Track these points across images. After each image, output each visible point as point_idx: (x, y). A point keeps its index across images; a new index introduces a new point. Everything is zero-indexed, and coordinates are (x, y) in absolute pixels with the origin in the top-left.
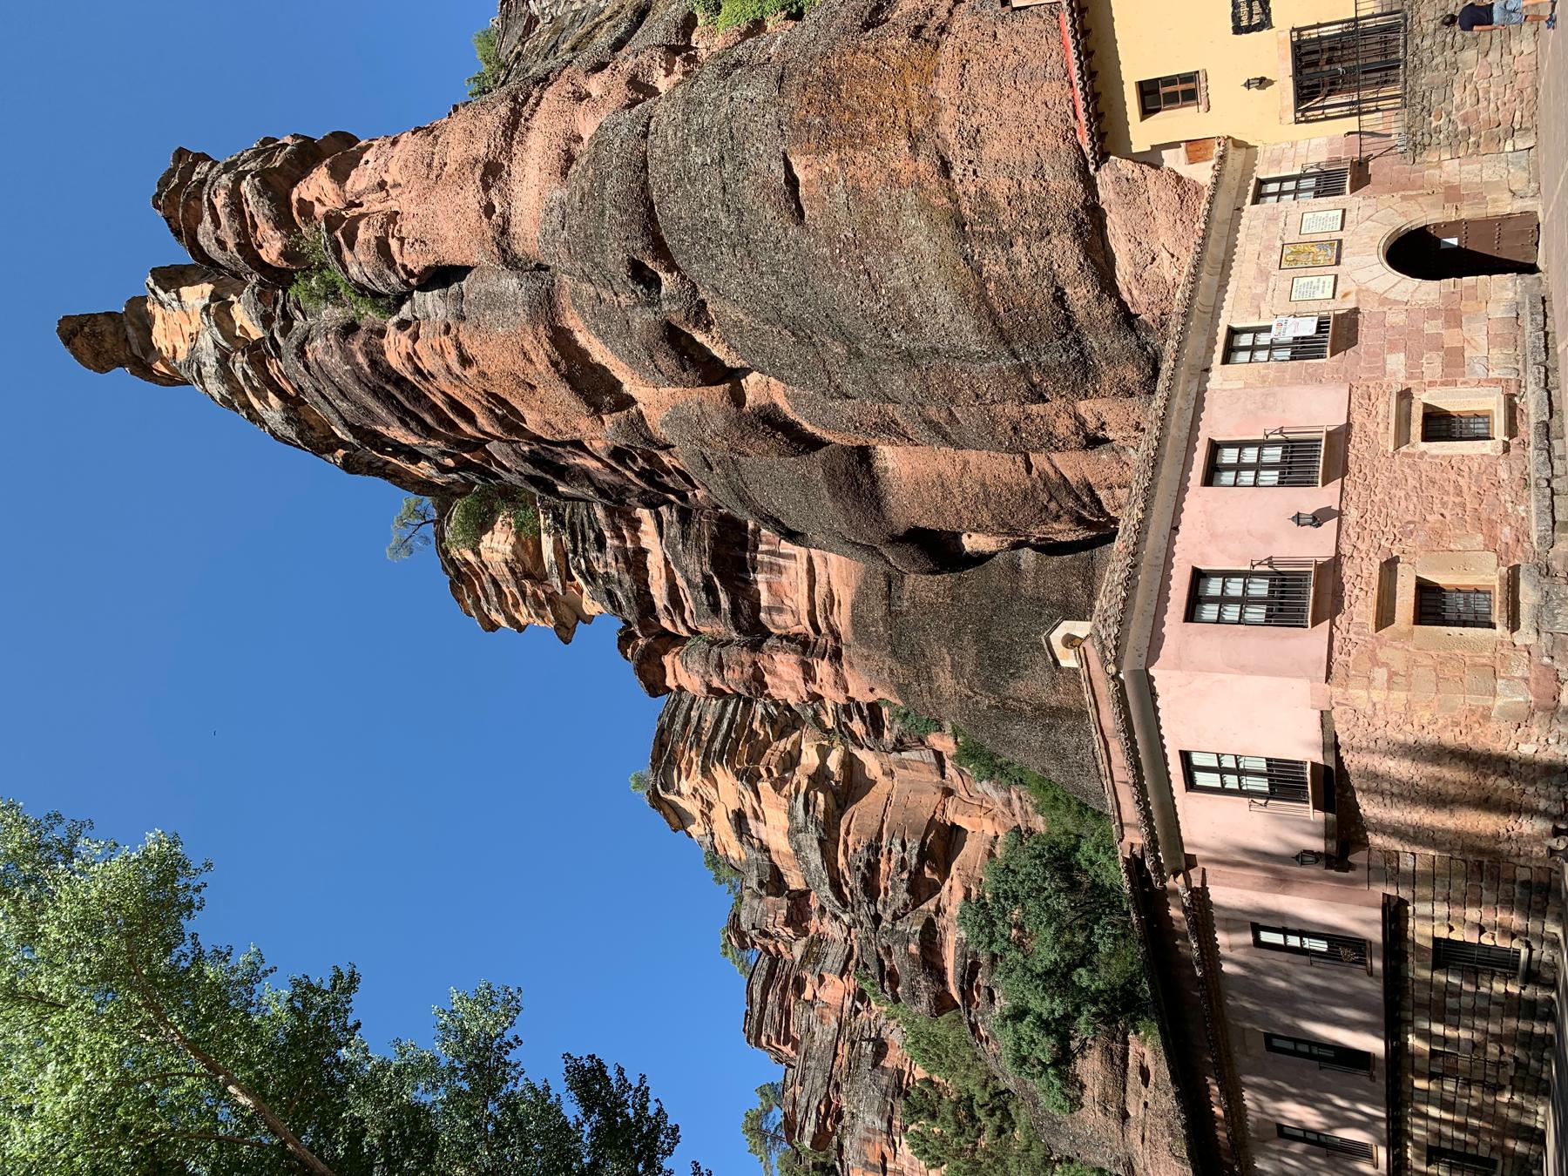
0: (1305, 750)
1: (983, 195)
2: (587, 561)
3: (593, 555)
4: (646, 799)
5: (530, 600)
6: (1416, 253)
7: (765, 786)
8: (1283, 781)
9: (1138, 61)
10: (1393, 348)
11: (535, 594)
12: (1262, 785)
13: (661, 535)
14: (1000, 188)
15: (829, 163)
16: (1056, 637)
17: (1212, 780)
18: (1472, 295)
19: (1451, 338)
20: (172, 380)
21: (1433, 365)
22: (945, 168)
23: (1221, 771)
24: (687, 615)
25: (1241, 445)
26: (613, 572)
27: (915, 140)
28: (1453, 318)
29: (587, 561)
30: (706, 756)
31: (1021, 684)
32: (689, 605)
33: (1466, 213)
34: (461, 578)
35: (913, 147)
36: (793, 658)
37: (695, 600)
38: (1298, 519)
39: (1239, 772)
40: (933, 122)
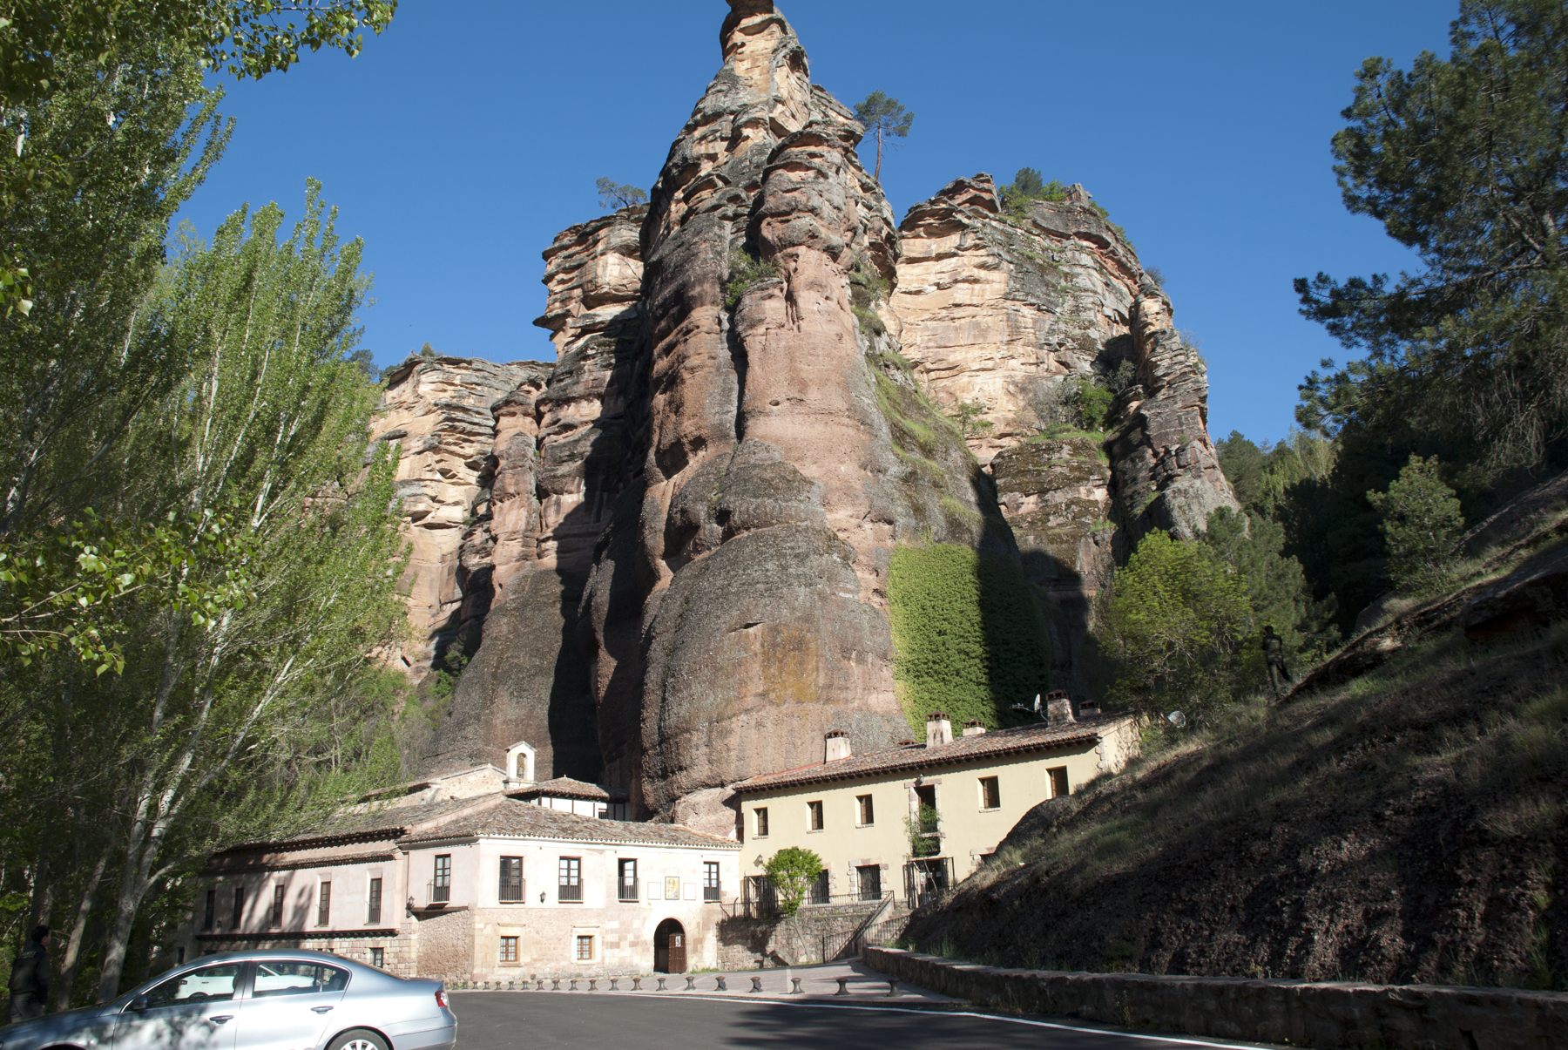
0: (454, 901)
1: (730, 732)
2: (593, 357)
3: (598, 360)
4: (410, 356)
5: (566, 294)
6: (669, 931)
7: (431, 458)
8: (442, 892)
9: (773, 804)
10: (622, 924)
11: (571, 298)
12: (439, 884)
13: (614, 418)
14: (733, 740)
15: (757, 647)
16: (523, 747)
17: (440, 865)
18: (646, 950)
19: (625, 944)
20: (724, 40)
21: (613, 938)
22: (747, 711)
23: (444, 869)
24: (553, 437)
25: (579, 869)
26: (586, 376)
27: (763, 695)
28: (633, 945)
29: (593, 357)
30: (448, 406)
31: (506, 699)
32: (561, 439)
33: (689, 948)
34: (586, 236)
35: (757, 695)
36: (522, 525)
37: (564, 445)
38: (543, 894)
39: (444, 876)
40: (771, 703)
